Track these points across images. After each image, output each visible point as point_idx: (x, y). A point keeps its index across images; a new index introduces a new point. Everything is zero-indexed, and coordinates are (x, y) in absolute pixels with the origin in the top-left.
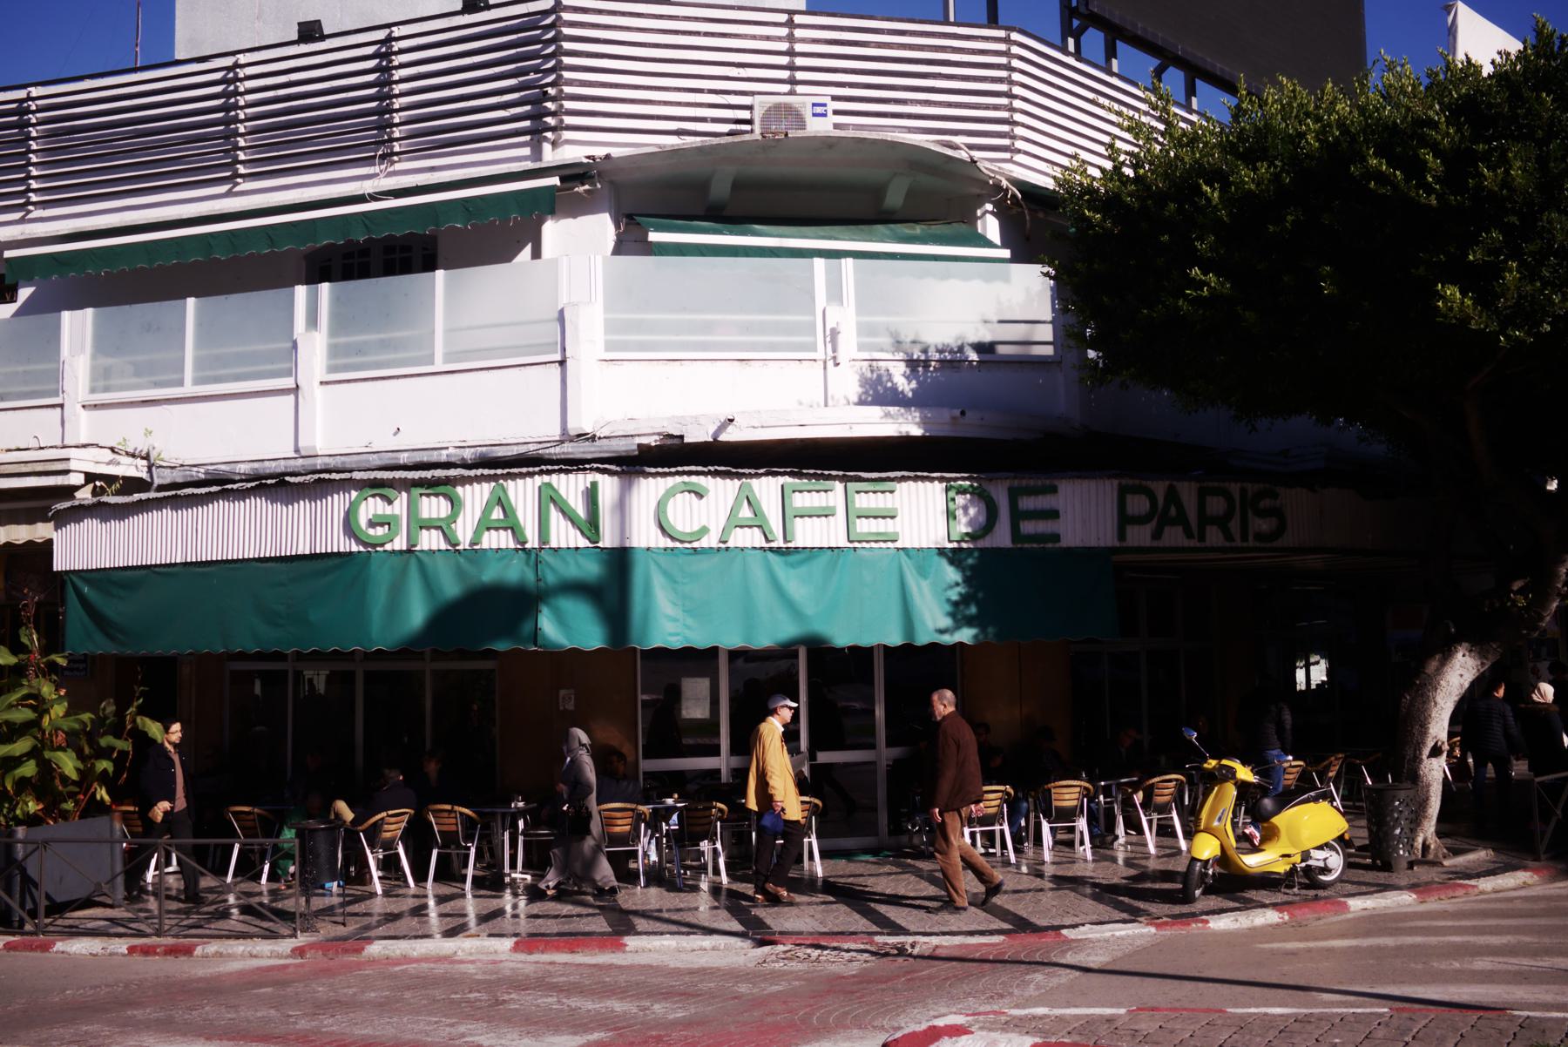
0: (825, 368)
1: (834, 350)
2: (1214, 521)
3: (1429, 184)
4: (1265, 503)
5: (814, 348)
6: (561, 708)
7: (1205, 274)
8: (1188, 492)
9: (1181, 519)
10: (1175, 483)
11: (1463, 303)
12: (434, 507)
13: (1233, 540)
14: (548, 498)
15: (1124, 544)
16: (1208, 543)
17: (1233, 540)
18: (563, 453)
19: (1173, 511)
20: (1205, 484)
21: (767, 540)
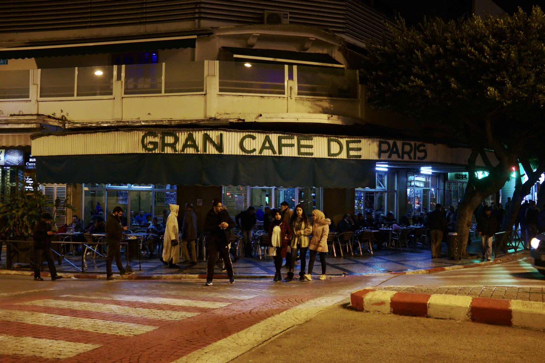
0: (287, 100)
1: (291, 95)
2: (406, 153)
3: (486, 56)
4: (421, 148)
5: (284, 93)
6: (198, 205)
7: (415, 78)
8: (399, 144)
9: (397, 152)
10: (396, 141)
11: (495, 92)
12: (170, 140)
13: (412, 159)
14: (207, 138)
15: (281, 155)
16: (404, 160)
17: (412, 159)
18: (205, 124)
19: (395, 150)
20: (404, 142)
21: (274, 153)
